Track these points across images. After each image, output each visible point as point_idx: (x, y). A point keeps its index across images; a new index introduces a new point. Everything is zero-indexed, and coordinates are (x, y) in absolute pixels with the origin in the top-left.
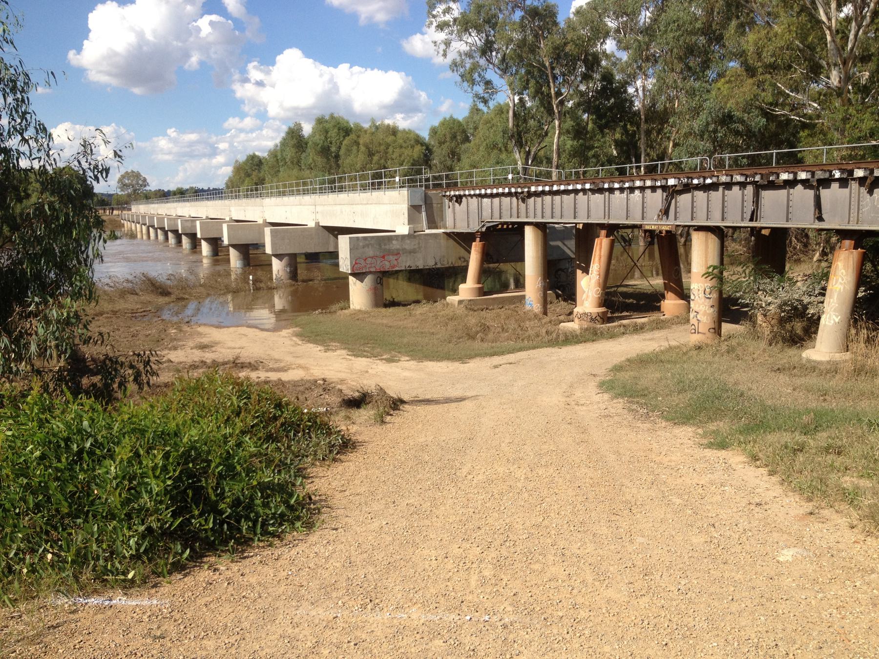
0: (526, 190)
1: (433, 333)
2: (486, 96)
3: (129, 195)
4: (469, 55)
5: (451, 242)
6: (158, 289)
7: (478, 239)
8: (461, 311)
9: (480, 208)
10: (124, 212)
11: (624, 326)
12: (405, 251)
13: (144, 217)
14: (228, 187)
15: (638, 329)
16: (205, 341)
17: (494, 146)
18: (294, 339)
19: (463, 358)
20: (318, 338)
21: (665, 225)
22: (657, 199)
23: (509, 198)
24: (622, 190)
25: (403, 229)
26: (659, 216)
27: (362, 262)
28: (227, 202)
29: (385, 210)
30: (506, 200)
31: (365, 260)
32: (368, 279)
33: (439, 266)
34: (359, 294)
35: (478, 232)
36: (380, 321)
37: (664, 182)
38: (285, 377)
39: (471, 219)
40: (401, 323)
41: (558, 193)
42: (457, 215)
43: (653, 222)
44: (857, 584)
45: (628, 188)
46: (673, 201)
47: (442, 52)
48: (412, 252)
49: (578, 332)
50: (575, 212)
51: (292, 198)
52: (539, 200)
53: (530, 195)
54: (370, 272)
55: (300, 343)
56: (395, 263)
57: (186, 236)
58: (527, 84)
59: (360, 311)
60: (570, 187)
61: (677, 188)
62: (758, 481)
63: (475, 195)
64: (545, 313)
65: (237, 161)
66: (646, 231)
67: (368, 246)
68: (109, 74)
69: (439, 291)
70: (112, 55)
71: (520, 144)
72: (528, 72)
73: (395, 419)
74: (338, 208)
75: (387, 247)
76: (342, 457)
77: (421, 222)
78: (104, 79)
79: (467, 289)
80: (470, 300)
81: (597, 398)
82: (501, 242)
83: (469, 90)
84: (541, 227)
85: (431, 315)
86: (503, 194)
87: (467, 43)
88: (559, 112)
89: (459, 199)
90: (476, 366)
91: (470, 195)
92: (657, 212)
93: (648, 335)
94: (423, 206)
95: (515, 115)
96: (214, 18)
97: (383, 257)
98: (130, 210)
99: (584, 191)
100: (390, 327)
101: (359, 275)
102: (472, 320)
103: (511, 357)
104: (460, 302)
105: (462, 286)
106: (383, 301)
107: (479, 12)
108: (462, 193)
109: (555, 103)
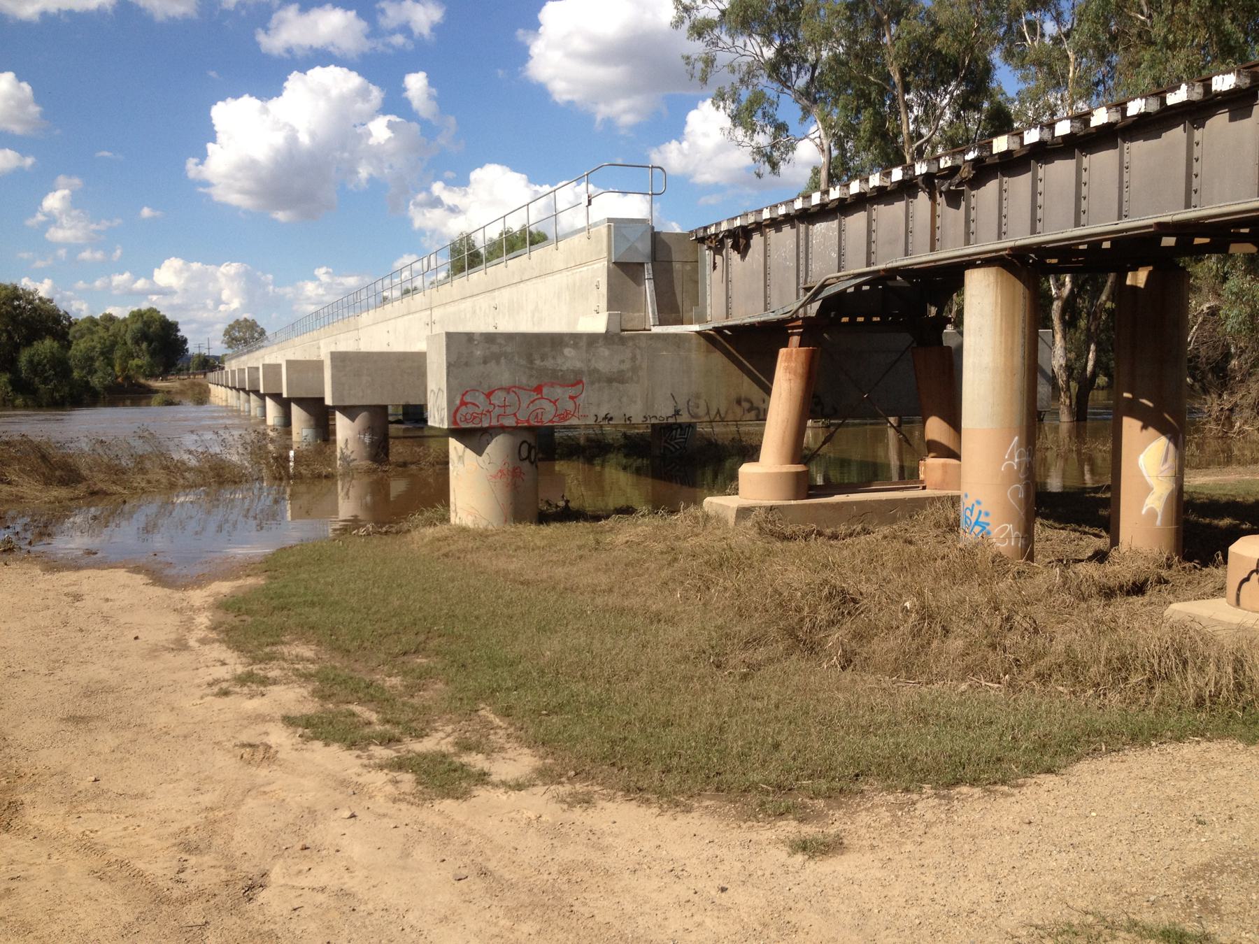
1: (657, 618)
7: (795, 340)
8: (746, 538)
9: (803, 252)
31: (489, 395)
32: (497, 448)
36: (501, 563)
40: (560, 572)
47: (698, 73)
48: (617, 379)
52: (1020, 184)
54: (503, 429)
56: (570, 406)
59: (463, 530)
67: (496, 358)
68: (243, 192)
69: (685, 490)
70: (250, 166)
74: (468, 304)
75: (549, 363)
77: (642, 308)
78: (235, 199)
79: (762, 479)
80: (771, 508)
83: (747, 140)
84: (1025, 265)
85: (660, 546)
94: (648, 268)
96: (393, 118)
97: (538, 389)
100: (526, 583)
101: (474, 437)
102: (792, 572)
104: (743, 512)
105: (746, 469)
106: (532, 503)
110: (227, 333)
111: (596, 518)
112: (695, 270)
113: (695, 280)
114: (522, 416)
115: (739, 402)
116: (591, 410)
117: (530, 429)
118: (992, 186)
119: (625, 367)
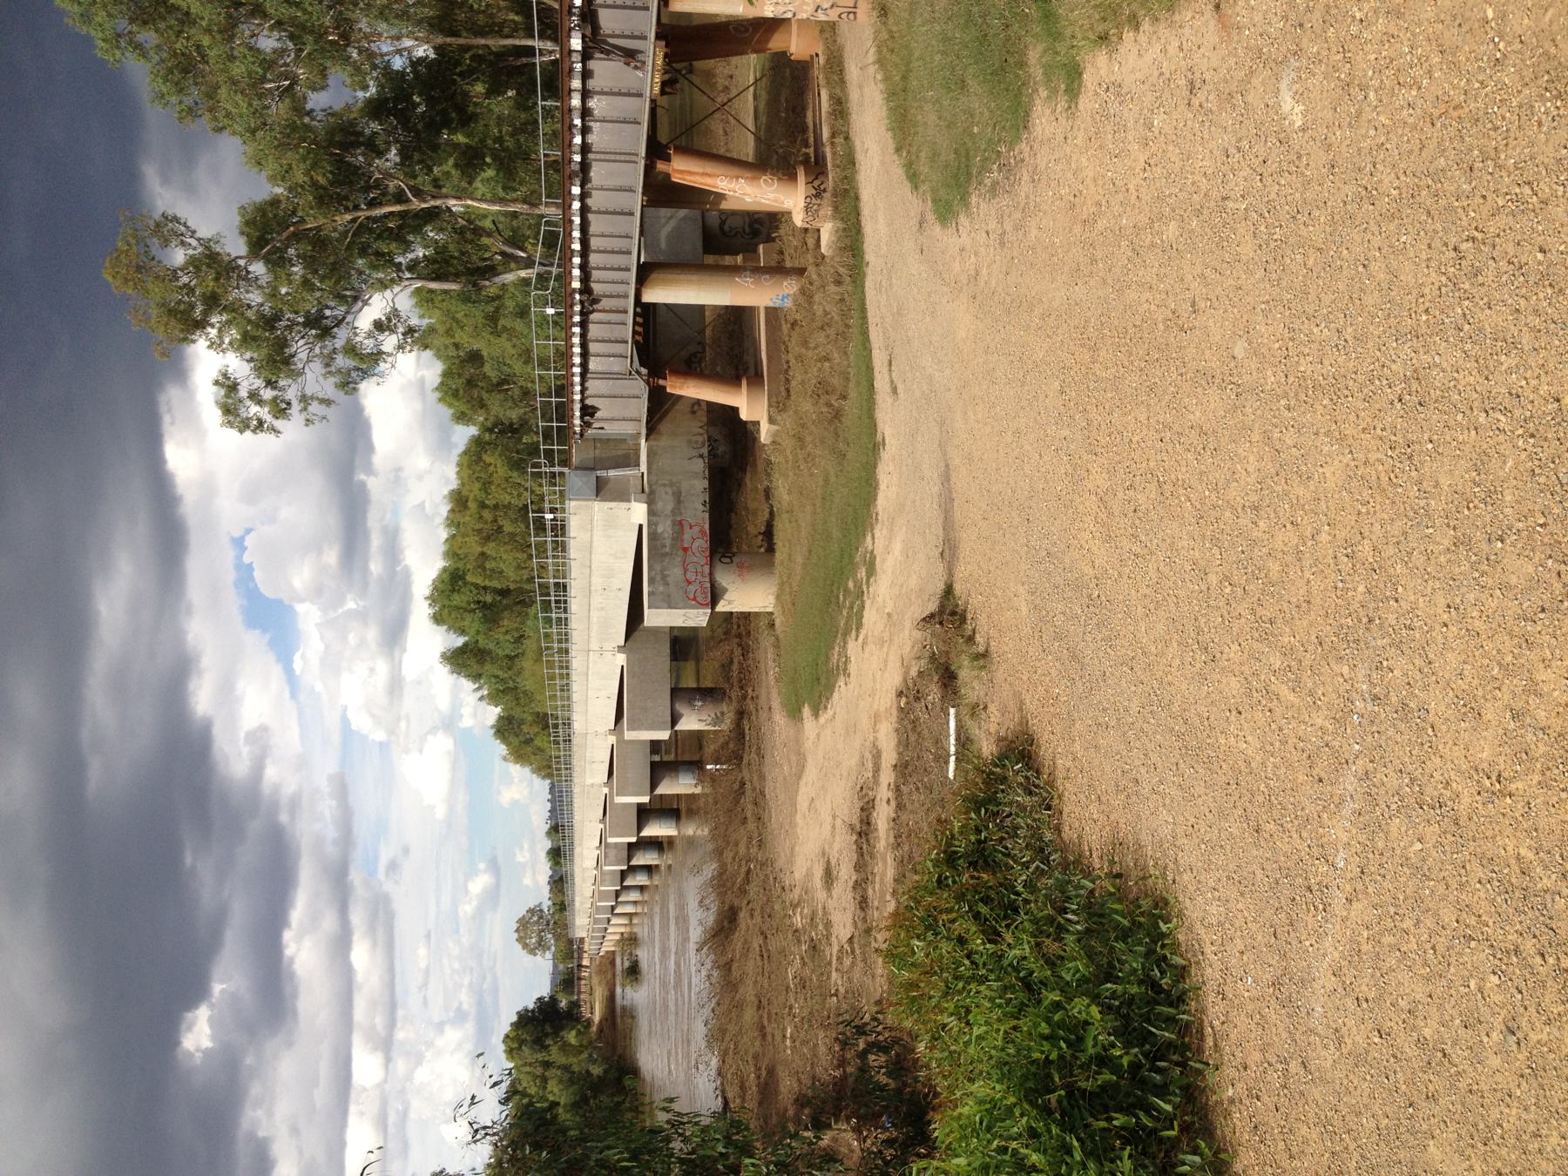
0: (577, 297)
1: (826, 481)
2: (401, 330)
3: (557, 938)
4: (328, 361)
5: (664, 427)
6: (724, 929)
7: (661, 382)
8: (787, 420)
9: (606, 375)
10: (586, 948)
11: (833, 135)
12: (677, 510)
13: (596, 921)
14: (549, 776)
15: (840, 109)
16: (818, 872)
17: (493, 319)
18: (822, 720)
19: (874, 448)
20: (823, 681)
21: (653, 53)
22: (606, 71)
23: (591, 326)
24: (585, 131)
25: (638, 512)
26: (636, 68)
27: (692, 588)
28: (576, 790)
29: (602, 541)
30: (594, 331)
31: (689, 583)
33: (705, 451)
34: (748, 595)
35: (648, 383)
36: (798, 568)
37: (576, 57)
38: (889, 757)
39: (626, 393)
41: (584, 241)
42: (616, 414)
43: (649, 79)
44: (1358, 16)
45: (583, 120)
46: (611, 41)
49: (840, 225)
50: (622, 213)
51: (575, 687)
52: (595, 274)
53: (586, 290)
54: (711, 574)
55: (830, 712)
56: (696, 529)
57: (636, 861)
58: (383, 255)
59: (778, 597)
60: (577, 220)
61: (588, 32)
62: (1148, 57)
63: (582, 384)
64: (801, 272)
65: (505, 759)
66: (663, 92)
67: (664, 577)
71: (491, 271)
72: (363, 252)
73: (984, 626)
75: (668, 542)
76: (1046, 770)
79: (748, 405)
80: (770, 405)
81: (965, 240)
82: (663, 344)
84: (645, 273)
86: (583, 336)
87: (308, 361)
88: (434, 197)
89: (588, 411)
90: (890, 419)
91: (582, 392)
92: (629, 69)
93: (854, 95)
94: (598, 473)
95: (438, 277)
97: (685, 550)
98: (582, 940)
99: (583, 196)
101: (715, 596)
103: (879, 358)
104: (771, 421)
107: (254, 339)
108: (577, 407)
109: (417, 205)
110: (532, 952)
111: (772, 513)
112: (600, 440)
113: (607, 441)
114: (703, 561)
115: (694, 413)
116: (698, 514)
117: (711, 556)
118: (593, 285)
119: (669, 490)
